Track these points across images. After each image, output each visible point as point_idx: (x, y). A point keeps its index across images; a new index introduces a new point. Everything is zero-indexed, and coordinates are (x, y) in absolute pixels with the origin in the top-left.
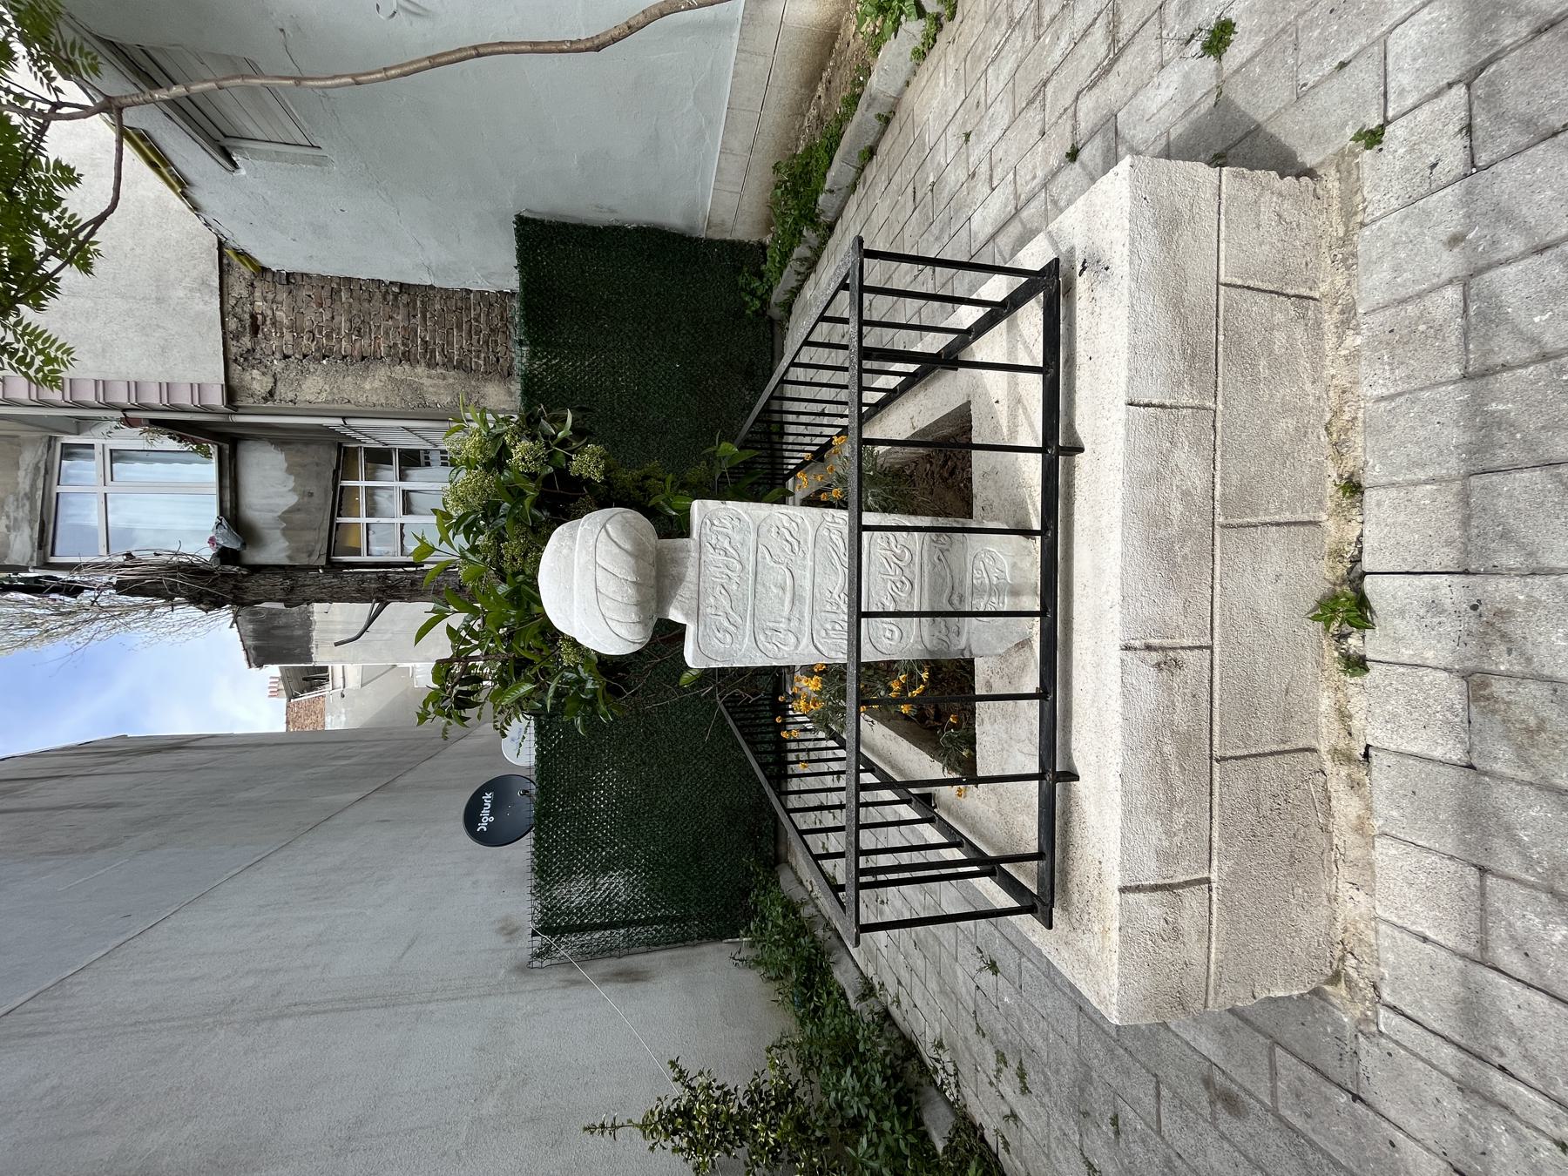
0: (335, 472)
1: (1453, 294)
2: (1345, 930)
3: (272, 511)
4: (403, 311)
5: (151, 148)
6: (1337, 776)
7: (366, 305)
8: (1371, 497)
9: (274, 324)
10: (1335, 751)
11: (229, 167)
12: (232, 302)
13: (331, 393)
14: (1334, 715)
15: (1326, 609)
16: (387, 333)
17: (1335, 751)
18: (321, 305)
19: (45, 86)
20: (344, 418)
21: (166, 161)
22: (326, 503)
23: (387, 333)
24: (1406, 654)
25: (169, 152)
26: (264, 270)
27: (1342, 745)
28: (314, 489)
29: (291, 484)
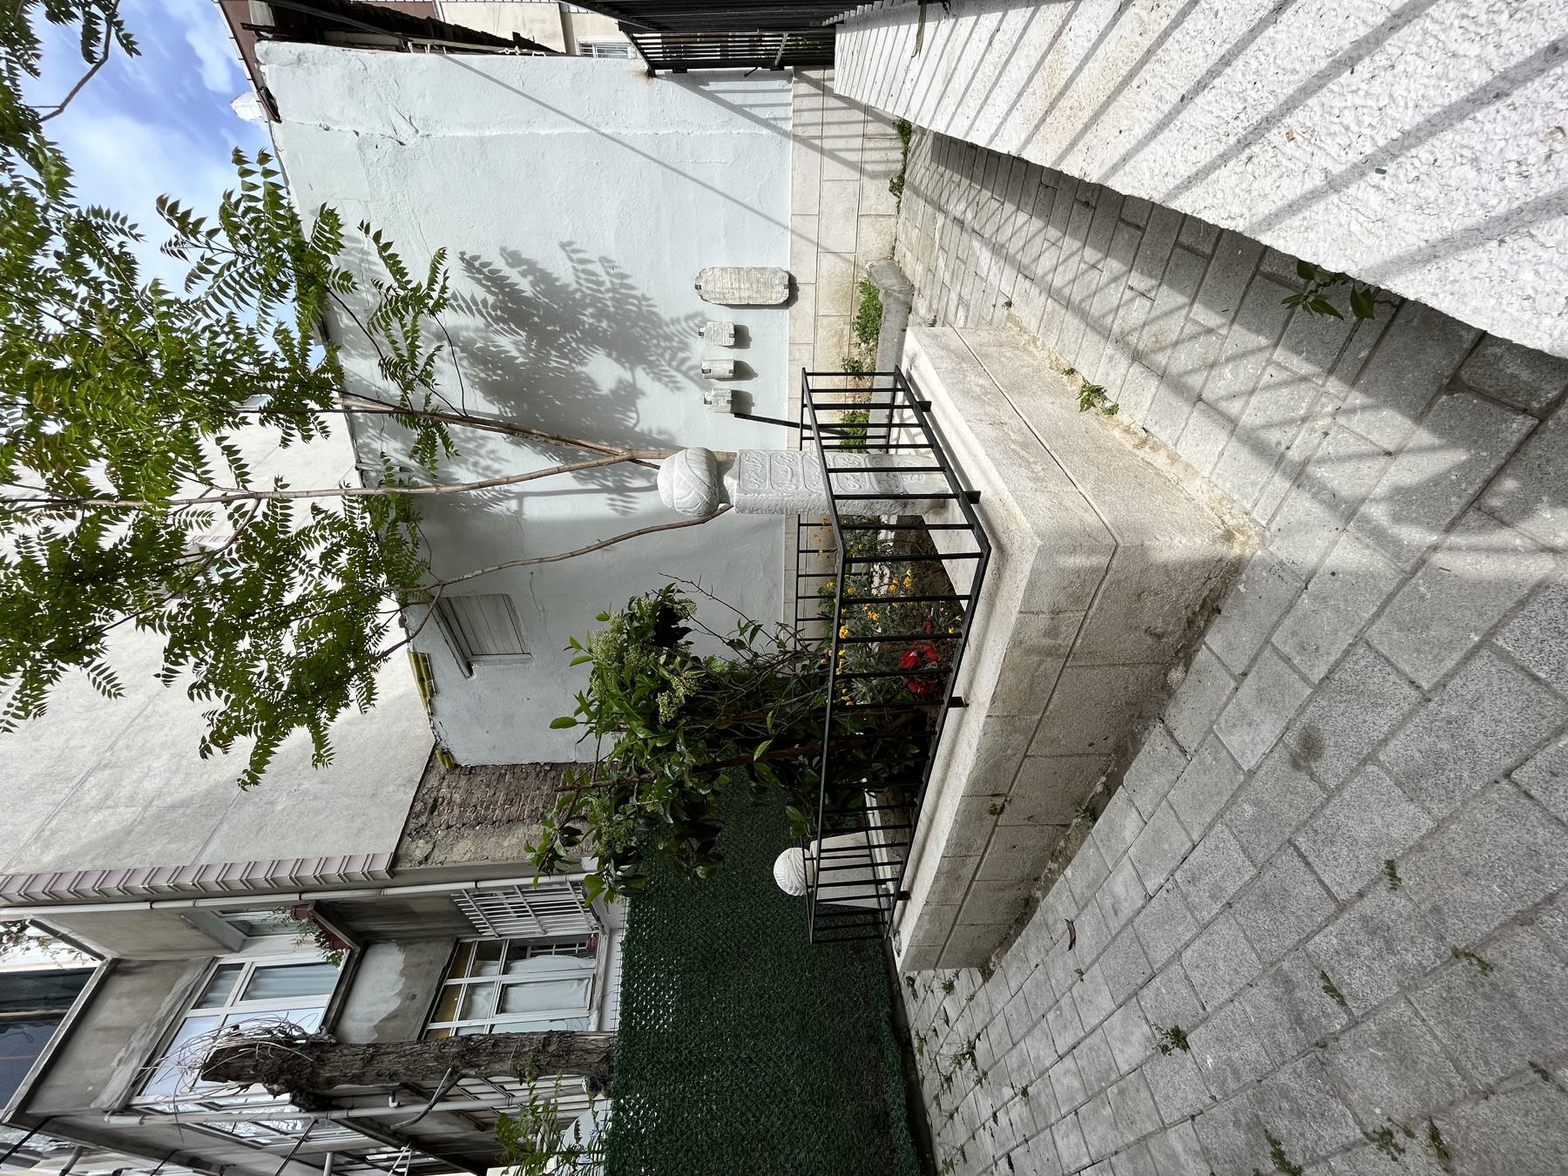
0: (445, 970)
1: (1050, 300)
2: (1213, 509)
3: (371, 1020)
4: (549, 782)
5: (426, 667)
6: (1145, 453)
7: (522, 782)
8: (1075, 367)
9: (449, 804)
10: (1136, 446)
11: (467, 674)
12: (424, 791)
13: (476, 852)
14: (1123, 435)
15: (1087, 403)
16: (532, 800)
17: (1136, 446)
18: (488, 786)
19: (499, 264)
20: (476, 881)
21: (430, 675)
22: (424, 1006)
23: (532, 800)
24: (1119, 382)
25: (435, 669)
26: (457, 766)
27: (1137, 442)
28: (418, 991)
29: (400, 987)
